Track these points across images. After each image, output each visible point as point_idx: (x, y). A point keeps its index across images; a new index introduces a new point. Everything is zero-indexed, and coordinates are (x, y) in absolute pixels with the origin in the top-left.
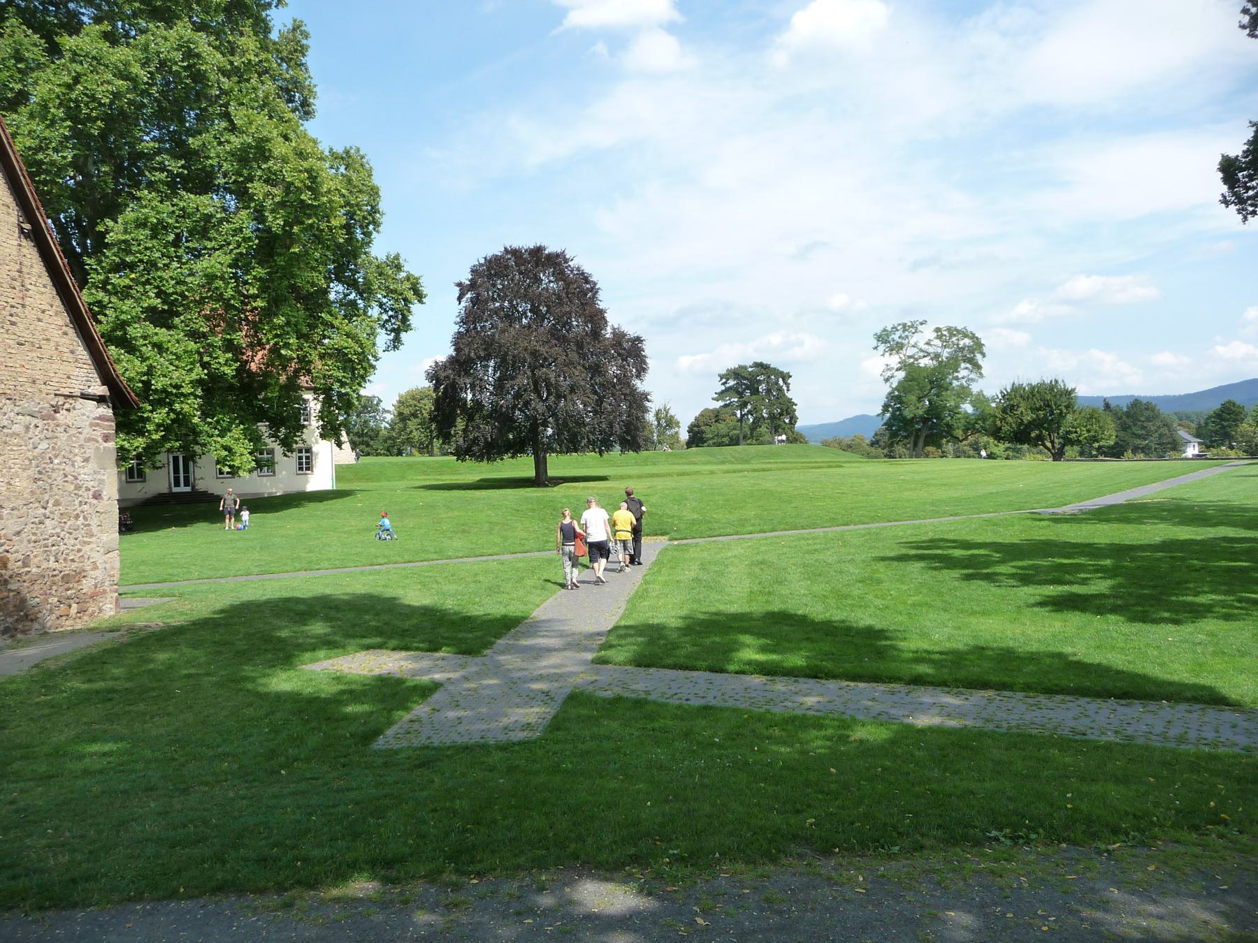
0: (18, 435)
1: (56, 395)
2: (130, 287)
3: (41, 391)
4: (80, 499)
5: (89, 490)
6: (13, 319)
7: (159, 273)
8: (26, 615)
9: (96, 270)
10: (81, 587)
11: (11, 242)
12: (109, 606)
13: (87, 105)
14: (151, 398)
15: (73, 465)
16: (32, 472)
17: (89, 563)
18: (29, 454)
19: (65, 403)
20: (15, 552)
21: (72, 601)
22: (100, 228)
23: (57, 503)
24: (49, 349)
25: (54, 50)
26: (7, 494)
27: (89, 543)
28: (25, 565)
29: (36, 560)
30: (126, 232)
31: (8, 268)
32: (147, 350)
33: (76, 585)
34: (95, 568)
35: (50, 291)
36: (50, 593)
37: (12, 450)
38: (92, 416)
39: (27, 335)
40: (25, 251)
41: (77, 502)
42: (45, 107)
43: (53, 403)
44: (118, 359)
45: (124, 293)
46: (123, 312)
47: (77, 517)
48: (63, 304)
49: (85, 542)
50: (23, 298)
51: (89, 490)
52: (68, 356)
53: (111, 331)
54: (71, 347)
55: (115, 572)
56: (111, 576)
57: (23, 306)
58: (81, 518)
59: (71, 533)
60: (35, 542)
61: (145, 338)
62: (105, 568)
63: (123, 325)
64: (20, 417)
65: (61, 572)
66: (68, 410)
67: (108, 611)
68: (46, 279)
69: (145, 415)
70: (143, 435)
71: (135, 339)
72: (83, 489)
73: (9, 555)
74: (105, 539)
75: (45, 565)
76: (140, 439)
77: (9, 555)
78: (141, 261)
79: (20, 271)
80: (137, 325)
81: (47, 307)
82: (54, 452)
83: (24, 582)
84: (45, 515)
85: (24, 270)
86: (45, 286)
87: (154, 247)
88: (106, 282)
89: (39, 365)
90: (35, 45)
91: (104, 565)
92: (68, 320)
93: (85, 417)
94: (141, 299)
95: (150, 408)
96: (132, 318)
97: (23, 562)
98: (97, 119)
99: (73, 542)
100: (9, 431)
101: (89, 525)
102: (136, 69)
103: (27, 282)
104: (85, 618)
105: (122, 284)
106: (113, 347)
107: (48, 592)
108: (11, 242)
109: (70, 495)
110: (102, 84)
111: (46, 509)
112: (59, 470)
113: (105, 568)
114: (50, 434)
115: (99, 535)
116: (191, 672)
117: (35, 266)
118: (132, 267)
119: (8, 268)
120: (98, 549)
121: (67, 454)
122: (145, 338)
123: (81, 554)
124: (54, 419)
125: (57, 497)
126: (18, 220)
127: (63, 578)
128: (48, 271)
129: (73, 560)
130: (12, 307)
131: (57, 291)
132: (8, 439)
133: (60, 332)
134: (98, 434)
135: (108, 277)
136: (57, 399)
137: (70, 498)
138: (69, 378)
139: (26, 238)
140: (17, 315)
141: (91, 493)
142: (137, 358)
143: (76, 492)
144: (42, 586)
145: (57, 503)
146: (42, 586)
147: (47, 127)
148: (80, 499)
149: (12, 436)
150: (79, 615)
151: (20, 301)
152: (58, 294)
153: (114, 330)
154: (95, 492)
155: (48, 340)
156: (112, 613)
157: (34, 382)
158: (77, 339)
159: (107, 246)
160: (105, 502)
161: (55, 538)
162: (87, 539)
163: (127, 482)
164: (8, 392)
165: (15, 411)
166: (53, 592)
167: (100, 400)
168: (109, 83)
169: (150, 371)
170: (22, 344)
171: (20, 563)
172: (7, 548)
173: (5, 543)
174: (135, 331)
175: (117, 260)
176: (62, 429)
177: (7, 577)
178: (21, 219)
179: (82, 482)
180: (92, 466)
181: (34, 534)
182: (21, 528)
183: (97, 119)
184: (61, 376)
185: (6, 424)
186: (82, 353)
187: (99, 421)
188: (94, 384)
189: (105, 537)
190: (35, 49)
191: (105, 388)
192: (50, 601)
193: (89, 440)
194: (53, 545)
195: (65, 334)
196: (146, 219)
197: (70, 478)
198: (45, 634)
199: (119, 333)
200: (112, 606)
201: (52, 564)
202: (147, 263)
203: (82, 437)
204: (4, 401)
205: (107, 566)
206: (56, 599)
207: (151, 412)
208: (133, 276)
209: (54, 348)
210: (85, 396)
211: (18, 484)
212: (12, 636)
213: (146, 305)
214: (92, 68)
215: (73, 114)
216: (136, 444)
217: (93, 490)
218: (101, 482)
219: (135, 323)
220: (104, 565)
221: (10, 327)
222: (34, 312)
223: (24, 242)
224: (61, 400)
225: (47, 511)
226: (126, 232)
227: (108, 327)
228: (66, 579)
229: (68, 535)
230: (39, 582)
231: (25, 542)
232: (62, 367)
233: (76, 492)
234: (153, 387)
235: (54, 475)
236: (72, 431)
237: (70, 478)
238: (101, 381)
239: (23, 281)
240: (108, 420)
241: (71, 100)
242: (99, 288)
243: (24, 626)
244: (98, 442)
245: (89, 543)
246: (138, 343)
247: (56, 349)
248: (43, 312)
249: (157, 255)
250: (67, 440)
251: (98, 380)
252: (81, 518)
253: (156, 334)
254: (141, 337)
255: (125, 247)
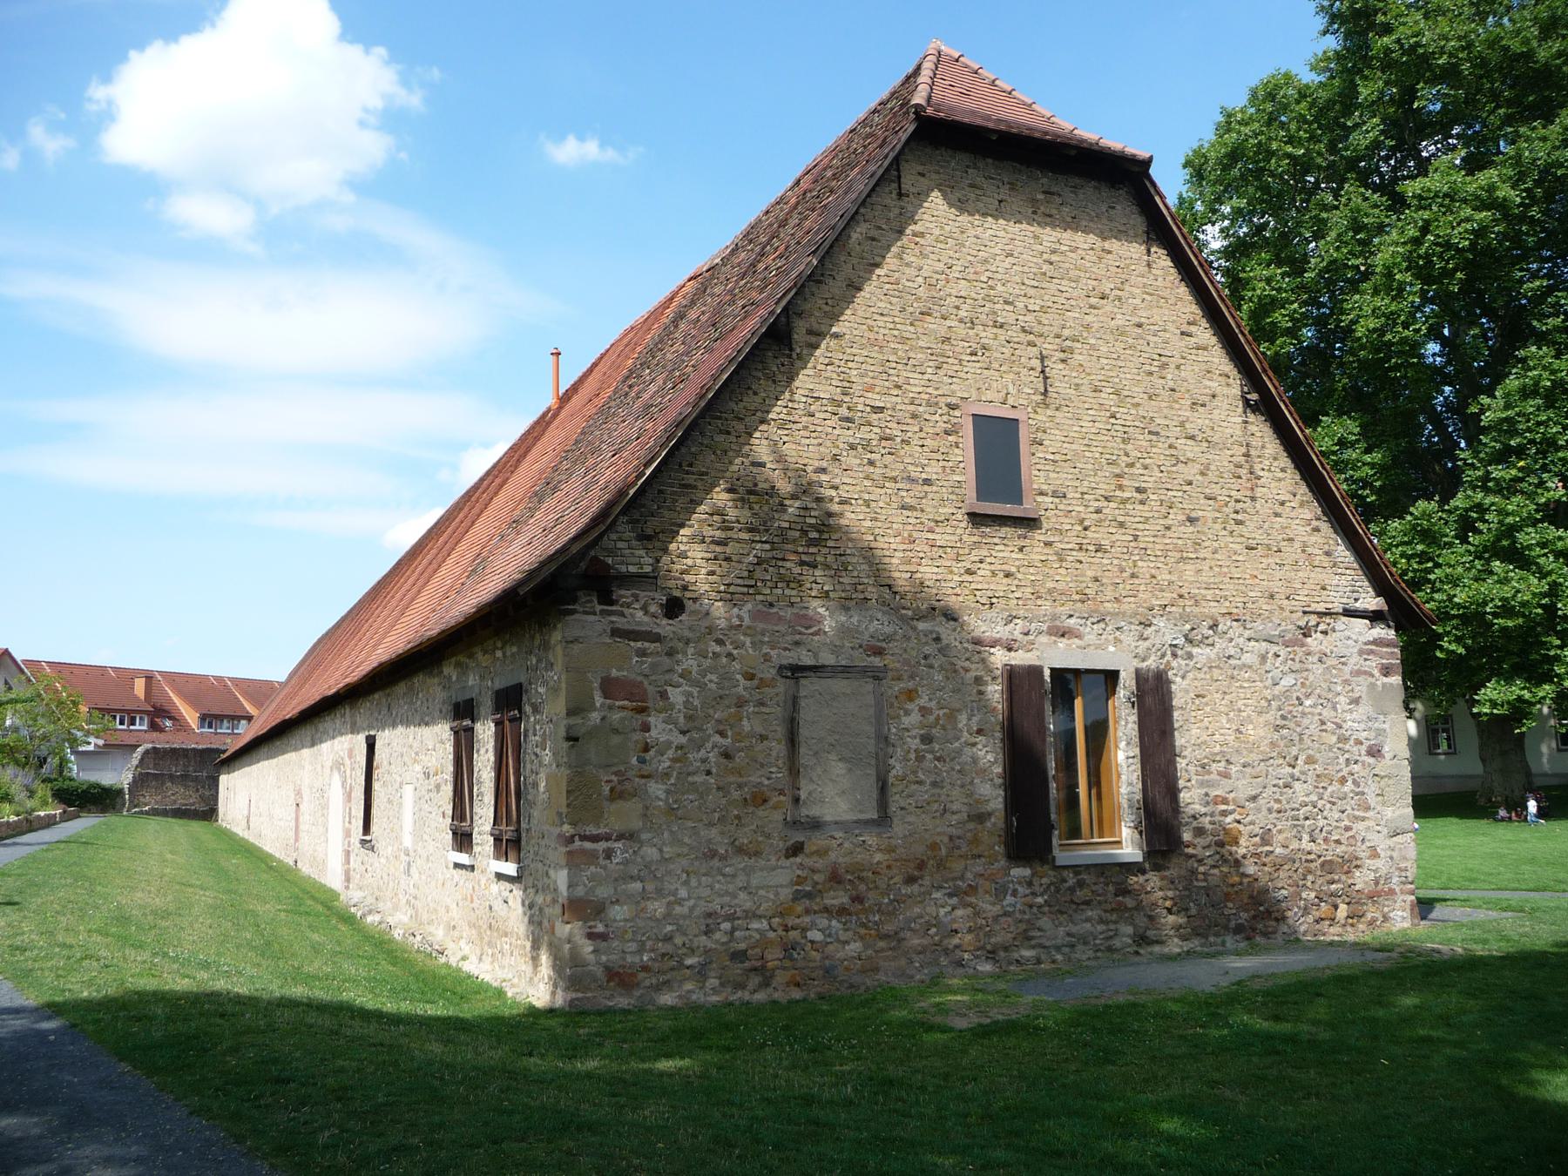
0: (1250, 667)
1: (1305, 613)
2: (1521, 480)
3: (1282, 609)
4: (1346, 756)
5: (1362, 743)
6: (1239, 517)
7: (1560, 454)
8: (1268, 912)
9: (1473, 464)
10: (1350, 881)
11: (1233, 420)
12: (1400, 913)
13: (1441, 257)
14: (1559, 628)
15: (1334, 708)
16: (1272, 716)
17: (1364, 847)
18: (1267, 693)
19: (1318, 624)
20: (1250, 824)
21: (1339, 901)
22: (1474, 409)
23: (1310, 760)
24: (1291, 553)
25: (1398, 203)
26: (1237, 745)
27: (1363, 819)
28: (1265, 841)
29: (1281, 837)
30: (1507, 407)
31: (1229, 453)
32: (1549, 562)
33: (1344, 877)
34: (1375, 854)
35: (1291, 477)
36: (1304, 885)
37: (1241, 687)
38: (1362, 639)
39: (1259, 536)
40: (1253, 428)
41: (1342, 760)
42: (1389, 275)
43: (1302, 623)
44: (1506, 578)
45: (1508, 489)
46: (1508, 514)
47: (1343, 781)
48: (1311, 490)
49: (1356, 818)
50: (1252, 489)
51: (1362, 743)
52: (1326, 561)
53: (1494, 542)
54: (1326, 547)
55: (1409, 864)
56: (1400, 869)
57: (1253, 499)
58: (1350, 783)
59: (1334, 804)
60: (1279, 812)
61: (1543, 545)
62: (1391, 858)
63: (1511, 531)
64: (1253, 643)
65: (1320, 857)
66: (1325, 633)
67: (1399, 920)
68: (1285, 461)
69: (1552, 653)
70: (1552, 682)
71: (1529, 547)
72: (1352, 742)
73: (1241, 827)
74: (1390, 814)
75: (1294, 845)
76: (1547, 687)
77: (1241, 827)
78: (1532, 442)
79: (1247, 455)
80: (1530, 530)
81: (1289, 497)
82: (1304, 690)
83: (1265, 865)
84: (1292, 776)
85: (1253, 452)
86: (1283, 470)
87: (1550, 419)
88: (1486, 478)
89: (1279, 575)
90: (1376, 206)
91: (1389, 853)
92: (1319, 511)
93: (1350, 642)
94: (1536, 493)
95: (1558, 642)
96: (1522, 520)
97: (1262, 839)
98: (1455, 270)
99: (1337, 815)
100: (1237, 662)
101: (1363, 793)
102: (1505, 192)
103: (1257, 467)
104: (1361, 927)
105: (1508, 477)
106: (1498, 563)
107: (1301, 883)
108: (1233, 420)
109: (1330, 750)
110: (1459, 224)
111: (1294, 767)
112: (1313, 714)
113: (1391, 858)
114: (1297, 666)
115: (1379, 808)
116: (1434, 1033)
117: (1268, 445)
118: (1520, 452)
119: (1229, 453)
120: (1379, 828)
121: (1324, 694)
122: (1543, 545)
123: (1350, 833)
124: (1303, 645)
125: (1310, 752)
126: (1242, 391)
127: (1323, 865)
128: (1286, 450)
129: (1338, 842)
130: (1238, 501)
131: (1301, 474)
132: (1235, 673)
133: (1308, 529)
134: (1373, 664)
135: (1488, 472)
136: (1306, 619)
137: (1331, 754)
138: (1324, 588)
139: (1254, 412)
140: (1245, 512)
141: (1364, 749)
142: (1533, 573)
143: (1340, 745)
144: (1290, 873)
145: (1310, 760)
146: (1290, 873)
147: (1393, 299)
148: (1346, 756)
149: (1241, 669)
150: (1350, 921)
151: (1249, 493)
152: (1303, 478)
153: (1498, 539)
154: (1370, 747)
155: (1291, 540)
156: (1406, 925)
157: (1272, 597)
158: (1334, 536)
159: (1485, 430)
160: (1387, 761)
161: (1309, 808)
162: (1361, 814)
163: (1559, 750)
164: (1235, 611)
165: (1246, 636)
166: (1309, 884)
167: (1375, 617)
168: (1467, 220)
169: (1554, 590)
170: (1253, 549)
171: (1258, 839)
172: (1238, 817)
173: (1234, 811)
174: (1528, 537)
175: (1498, 446)
176: (1315, 659)
177: (1239, 857)
178: (1246, 389)
179: (1349, 733)
180: (1364, 709)
181: (1278, 801)
182: (1258, 791)
183: (1455, 270)
184: (1313, 587)
185: (1232, 653)
186: (1343, 553)
187: (1374, 647)
188: (1363, 595)
189: (1389, 813)
190: (1377, 211)
191: (1381, 600)
192: (1304, 895)
193: (1358, 673)
194: (1307, 818)
195: (1317, 530)
196: (1537, 384)
197: (1330, 726)
198: (1293, 942)
199: (1505, 543)
200: (1405, 914)
201: (1306, 844)
202: (1540, 443)
203: (1347, 669)
204: (1229, 623)
205: (1395, 855)
206: (1313, 895)
207: (1561, 647)
208: (1522, 464)
209: (1299, 551)
210: (1349, 613)
211: (1252, 732)
212: (1248, 938)
213: (1543, 500)
214: (1443, 210)
215: (1425, 274)
216: (1541, 694)
217: (1366, 744)
218: (1380, 732)
219: (1528, 526)
220: (1389, 853)
221: (1235, 527)
222: (1269, 505)
223: (1252, 418)
224: (1313, 620)
225: (1296, 771)
226: (1507, 407)
227: (1491, 537)
228: (1328, 867)
229: (1329, 806)
230: (1286, 867)
231: (1265, 812)
232: (1313, 575)
233: (1340, 745)
234: (1560, 613)
235: (1306, 722)
236: (1330, 662)
237: (1330, 726)
238: (1375, 590)
239: (1252, 467)
240: (1388, 646)
241: (1420, 257)
242: (1478, 487)
243: (1265, 926)
244: (1373, 676)
245: (1363, 819)
246: (1533, 554)
247: (1303, 551)
248: (1282, 504)
249: (1554, 430)
250: (1323, 674)
251: (1370, 589)
252: (1350, 783)
253: (1560, 538)
254: (1538, 544)
255: (1508, 427)
